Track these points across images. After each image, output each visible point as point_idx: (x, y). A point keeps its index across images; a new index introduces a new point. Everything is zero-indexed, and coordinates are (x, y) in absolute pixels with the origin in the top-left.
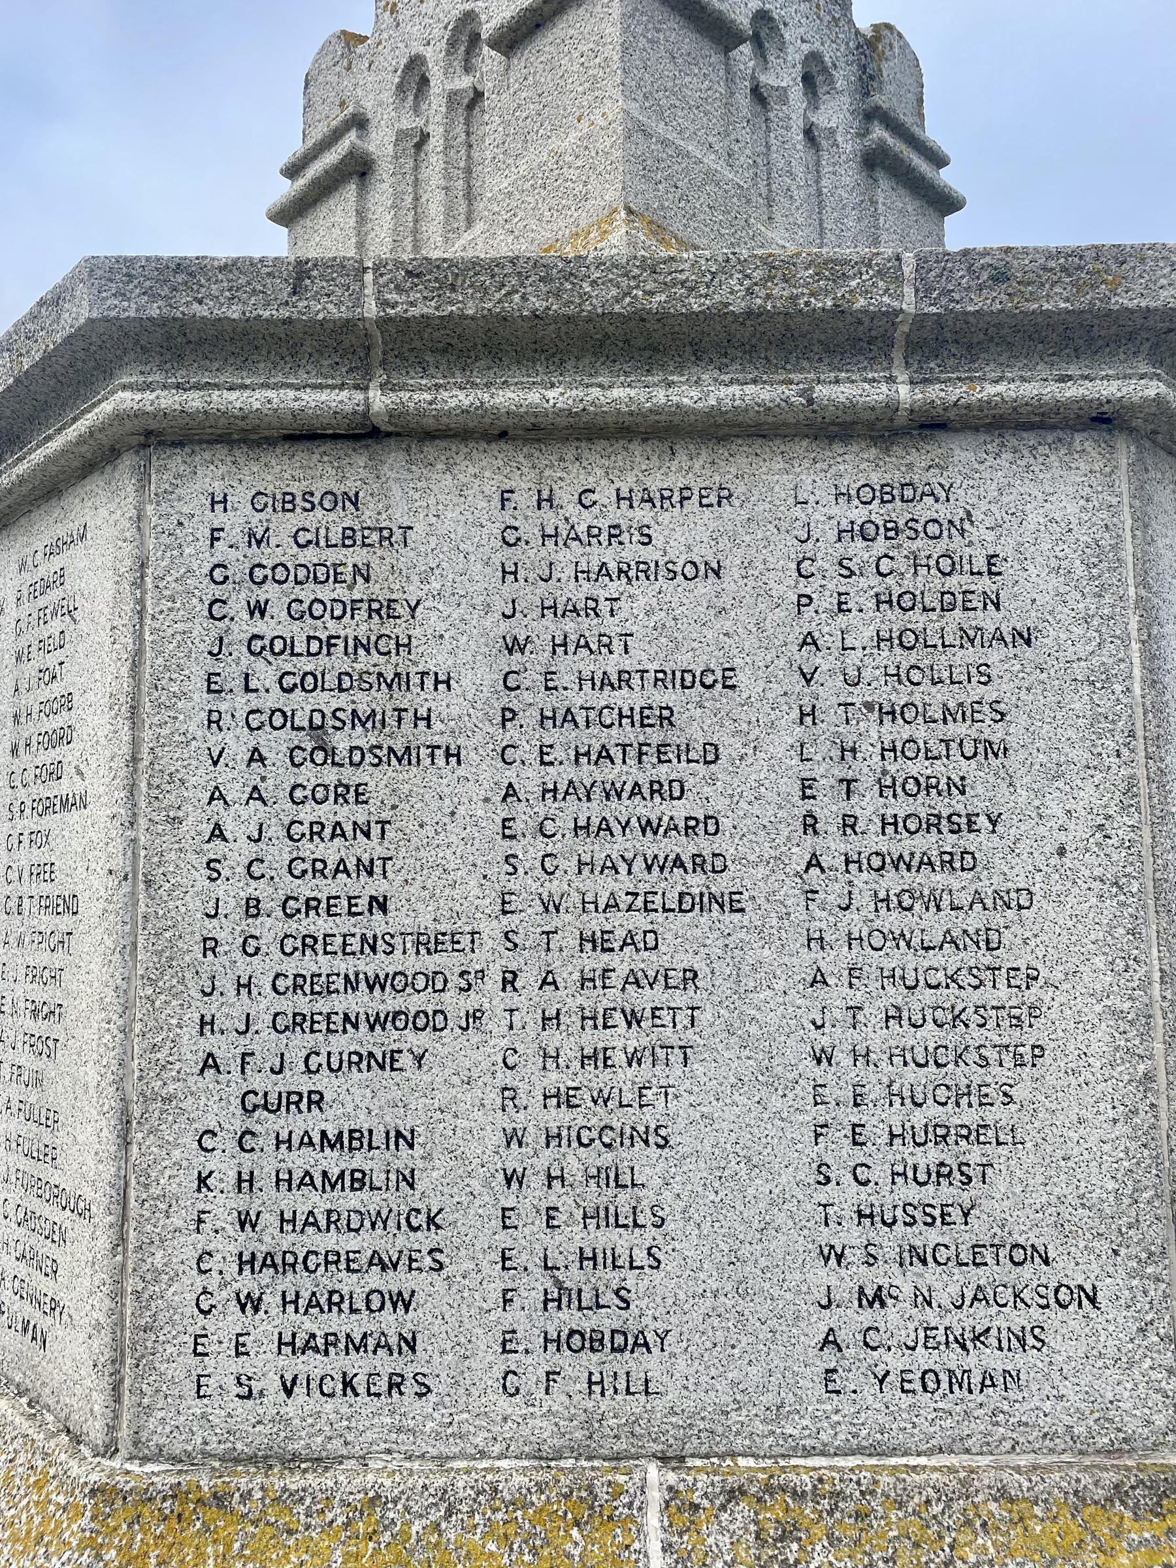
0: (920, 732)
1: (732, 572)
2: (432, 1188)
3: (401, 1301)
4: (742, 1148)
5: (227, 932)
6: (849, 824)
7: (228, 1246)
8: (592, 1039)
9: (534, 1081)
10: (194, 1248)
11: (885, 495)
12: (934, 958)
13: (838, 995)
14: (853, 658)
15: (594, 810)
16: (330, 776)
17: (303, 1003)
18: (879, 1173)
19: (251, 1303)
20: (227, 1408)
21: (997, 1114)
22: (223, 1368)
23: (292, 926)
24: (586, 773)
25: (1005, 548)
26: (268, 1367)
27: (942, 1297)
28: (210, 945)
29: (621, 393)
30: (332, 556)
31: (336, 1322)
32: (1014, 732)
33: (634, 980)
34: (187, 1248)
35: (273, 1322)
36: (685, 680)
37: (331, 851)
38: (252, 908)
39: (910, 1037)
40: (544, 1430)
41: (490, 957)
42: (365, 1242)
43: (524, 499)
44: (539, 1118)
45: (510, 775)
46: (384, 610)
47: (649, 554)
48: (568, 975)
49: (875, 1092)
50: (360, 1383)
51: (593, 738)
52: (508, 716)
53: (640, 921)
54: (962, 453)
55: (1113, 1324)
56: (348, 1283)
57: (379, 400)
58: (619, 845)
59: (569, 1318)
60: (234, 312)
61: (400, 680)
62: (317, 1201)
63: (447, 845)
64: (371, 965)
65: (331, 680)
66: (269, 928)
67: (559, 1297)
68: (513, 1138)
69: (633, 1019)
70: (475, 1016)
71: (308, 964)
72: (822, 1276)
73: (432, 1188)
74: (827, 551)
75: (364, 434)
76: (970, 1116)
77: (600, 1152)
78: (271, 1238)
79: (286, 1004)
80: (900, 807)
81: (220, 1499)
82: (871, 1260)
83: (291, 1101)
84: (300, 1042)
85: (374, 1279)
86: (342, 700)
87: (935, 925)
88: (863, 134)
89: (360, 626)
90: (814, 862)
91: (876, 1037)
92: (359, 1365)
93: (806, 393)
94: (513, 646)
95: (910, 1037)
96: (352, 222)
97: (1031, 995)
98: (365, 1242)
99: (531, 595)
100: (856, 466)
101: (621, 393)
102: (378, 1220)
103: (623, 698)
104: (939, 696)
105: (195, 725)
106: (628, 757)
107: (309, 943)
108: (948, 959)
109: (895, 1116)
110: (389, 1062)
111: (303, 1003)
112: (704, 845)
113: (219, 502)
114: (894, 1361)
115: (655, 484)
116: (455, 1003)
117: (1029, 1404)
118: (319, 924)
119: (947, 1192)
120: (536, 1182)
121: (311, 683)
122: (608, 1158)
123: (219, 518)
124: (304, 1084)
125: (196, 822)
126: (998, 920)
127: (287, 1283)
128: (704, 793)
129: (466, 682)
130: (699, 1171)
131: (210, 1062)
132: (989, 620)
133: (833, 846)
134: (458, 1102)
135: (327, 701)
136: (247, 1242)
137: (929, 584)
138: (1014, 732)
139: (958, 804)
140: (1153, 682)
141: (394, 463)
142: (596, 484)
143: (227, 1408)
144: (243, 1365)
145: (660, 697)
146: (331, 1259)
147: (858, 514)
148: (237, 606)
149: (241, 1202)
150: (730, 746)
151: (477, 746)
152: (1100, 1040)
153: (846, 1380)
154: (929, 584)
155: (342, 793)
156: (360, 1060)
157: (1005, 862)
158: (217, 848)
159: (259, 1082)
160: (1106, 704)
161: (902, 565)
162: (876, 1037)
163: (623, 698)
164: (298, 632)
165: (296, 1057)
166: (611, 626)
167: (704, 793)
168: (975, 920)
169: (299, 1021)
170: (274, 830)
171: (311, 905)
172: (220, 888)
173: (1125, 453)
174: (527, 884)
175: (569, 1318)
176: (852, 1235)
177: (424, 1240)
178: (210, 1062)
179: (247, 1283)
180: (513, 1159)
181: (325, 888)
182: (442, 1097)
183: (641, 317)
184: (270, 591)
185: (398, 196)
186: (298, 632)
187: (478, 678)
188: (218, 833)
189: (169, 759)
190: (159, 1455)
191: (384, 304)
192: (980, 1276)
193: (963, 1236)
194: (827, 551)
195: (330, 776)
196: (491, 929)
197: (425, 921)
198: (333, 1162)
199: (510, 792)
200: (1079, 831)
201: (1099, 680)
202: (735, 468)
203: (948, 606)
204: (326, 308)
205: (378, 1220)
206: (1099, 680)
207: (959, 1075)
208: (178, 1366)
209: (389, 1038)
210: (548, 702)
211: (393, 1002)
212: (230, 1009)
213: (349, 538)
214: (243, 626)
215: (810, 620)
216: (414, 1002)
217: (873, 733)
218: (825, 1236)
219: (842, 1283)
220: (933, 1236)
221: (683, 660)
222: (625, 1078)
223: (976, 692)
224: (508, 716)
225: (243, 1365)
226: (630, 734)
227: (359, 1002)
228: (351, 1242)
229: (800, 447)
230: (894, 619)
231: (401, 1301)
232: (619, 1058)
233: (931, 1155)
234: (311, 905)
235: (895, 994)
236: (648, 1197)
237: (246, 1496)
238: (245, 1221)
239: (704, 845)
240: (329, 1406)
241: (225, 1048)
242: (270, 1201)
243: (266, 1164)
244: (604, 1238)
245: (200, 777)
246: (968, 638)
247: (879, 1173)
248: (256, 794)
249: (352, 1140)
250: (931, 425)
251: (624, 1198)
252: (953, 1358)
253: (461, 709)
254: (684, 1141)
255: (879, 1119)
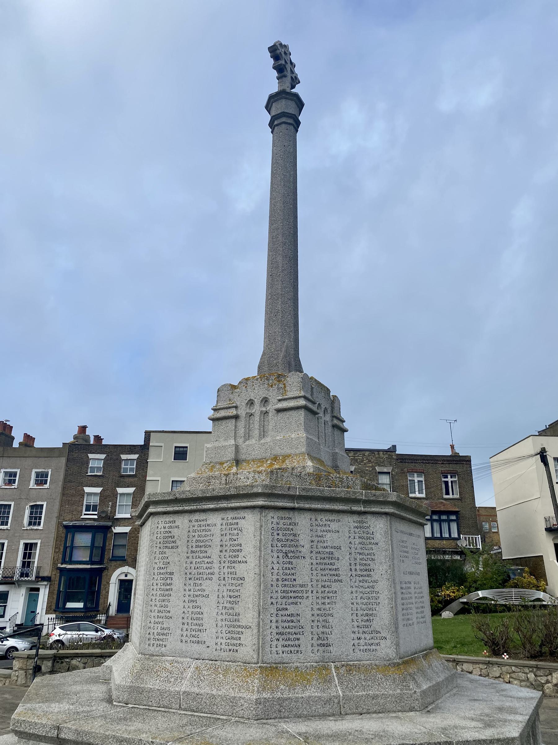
0: (364, 557)
1: (340, 532)
2: (302, 622)
3: (298, 639)
4: (342, 617)
5: (274, 583)
6: (356, 570)
7: (275, 631)
8: (323, 601)
9: (316, 607)
10: (270, 632)
11: (359, 522)
12: (366, 590)
13: (354, 595)
14: (356, 545)
15: (323, 567)
16: (288, 560)
17: (285, 594)
18: (360, 621)
19: (278, 640)
20: (275, 656)
21: (374, 612)
22: (274, 649)
23: (283, 583)
24: (322, 561)
25: (374, 531)
26: (280, 649)
27: (367, 638)
28: (272, 585)
29: (328, 506)
30: (288, 527)
31: (290, 643)
32: (376, 557)
33: (328, 592)
34: (269, 632)
35: (281, 642)
36: (335, 547)
37: (288, 572)
38: (278, 580)
39: (364, 601)
40: (317, 658)
41: (309, 588)
42: (293, 630)
43: (313, 519)
44: (316, 612)
45: (312, 561)
46: (295, 535)
47: (329, 529)
48: (320, 591)
49: (359, 609)
50: (293, 652)
51: (323, 556)
52: (312, 552)
53: (329, 583)
54: (369, 517)
55: (388, 642)
56: (291, 637)
57: (297, 505)
58: (327, 572)
59: (320, 642)
60: (280, 493)
61: (297, 546)
62: (287, 624)
63: (304, 571)
64: (294, 589)
65: (288, 546)
66: (280, 583)
67: (319, 638)
68: (313, 615)
69: (328, 598)
70: (308, 597)
71: (285, 589)
72: (353, 635)
73: (302, 622)
74: (352, 530)
75: (293, 509)
76: (371, 612)
77: (323, 617)
78: (281, 630)
79: (282, 595)
80: (362, 568)
81: (277, 668)
82: (359, 633)
83: (283, 609)
84: (284, 600)
85: (294, 636)
86: (289, 549)
87: (366, 585)
88: (332, 420)
89: (291, 537)
90: (351, 575)
91: (359, 601)
92: (292, 649)
93: (351, 508)
94: (312, 541)
95: (364, 601)
96: (234, 428)
97: (378, 595)
98: (293, 630)
99: (314, 534)
100: (356, 518)
101: (328, 506)
102: (295, 627)
103: (327, 550)
104: (366, 552)
105: (270, 552)
106: (326, 559)
107: (285, 586)
108: (368, 590)
109: (362, 612)
110: (296, 603)
111: (285, 594)
112: (337, 572)
113: (273, 518)
114: (362, 648)
115: (330, 518)
116: (305, 595)
117: (379, 654)
118: (287, 583)
119: (368, 623)
120: (316, 622)
121: (285, 546)
122: (325, 618)
123: (273, 520)
124: (285, 607)
125: (270, 567)
126: (374, 584)
127: (283, 637)
128: (337, 565)
129: (306, 547)
130: (337, 620)
131: (272, 603)
132: (372, 541)
133: (354, 573)
134: (305, 609)
135: (288, 549)
136: (277, 630)
137: (365, 535)
138: (376, 557)
139: (369, 567)
140: (392, 551)
141: (296, 513)
142: (323, 518)
143: (275, 656)
144: (277, 649)
145: (332, 550)
146: (289, 633)
147: (356, 525)
148: (275, 534)
149: (276, 624)
150: (341, 558)
151: (308, 556)
152: (386, 602)
153: (356, 651)
154: (365, 535)
155: (289, 563)
156: (292, 603)
157: (376, 576)
158: (273, 571)
159: (279, 606)
160: (387, 554)
161: (362, 532)
162: (359, 601)
163: (327, 550)
164: (283, 538)
165: (284, 603)
166: (325, 539)
167: (337, 565)
168: (371, 584)
169: (284, 597)
170: (280, 568)
171: (285, 580)
172: (273, 577)
173: (389, 518)
174: (314, 578)
175: (320, 642)
176: (356, 629)
177: (301, 630)
178: (272, 603)
179: (277, 637)
180: (313, 618)
181: (287, 577)
182: (304, 609)
183: (331, 497)
184: (279, 532)
185: (246, 425)
186: (283, 538)
187: (307, 546)
188: (273, 568)
189: (266, 557)
190: (265, 663)
191: (299, 493)
192: (372, 635)
193: (370, 629)
194: (352, 530)
195: (288, 560)
196: (310, 584)
197: (301, 583)
198: (289, 618)
199: (312, 564)
200: (384, 572)
201: (386, 550)
202: (341, 517)
203: (367, 538)
204: (291, 493)
205: (295, 627)
206: (386, 550)
207: (370, 606)
208: (268, 649)
209: (296, 600)
210: (317, 550)
211: (297, 595)
212: (275, 595)
213: (290, 524)
214: (276, 537)
215: (351, 540)
216: (300, 595)
217: (359, 557)
218: (353, 630)
219: (355, 636)
220: (367, 630)
221: (334, 545)
222: (328, 606)
223: (371, 551)
224: (312, 552)
225: (277, 649)
226: (327, 555)
227: (292, 595)
228: (291, 630)
229: (349, 515)
230: (361, 540)
231: (298, 639)
232: (327, 604)
233: (366, 618)
234: (285, 580)
235: (361, 595)
236: (330, 624)
237: (280, 667)
238: (277, 627)
239: (337, 572)
240: (289, 655)
241: (274, 601)
242: (280, 624)
243: (280, 619)
244: (325, 630)
245: (270, 560)
246: (370, 543)
247: (360, 621)
248: (278, 563)
249: (292, 615)
250: (365, 513)
251: (327, 624)
252: (369, 647)
253: (305, 551)
254: (335, 616)
255: (360, 612)
